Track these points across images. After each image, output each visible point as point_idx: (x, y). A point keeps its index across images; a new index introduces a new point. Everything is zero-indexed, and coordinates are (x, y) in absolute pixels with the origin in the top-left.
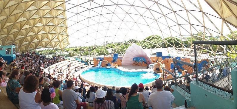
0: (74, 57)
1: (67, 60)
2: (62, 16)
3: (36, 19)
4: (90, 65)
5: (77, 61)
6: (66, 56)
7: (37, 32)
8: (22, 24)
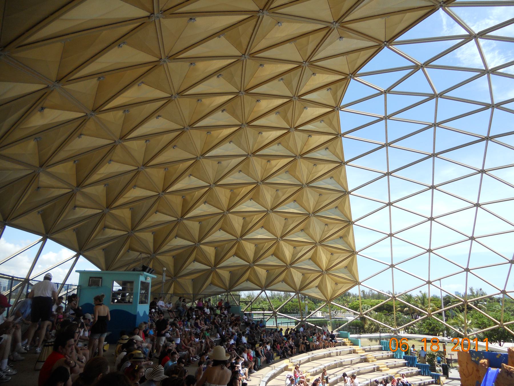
0: (377, 335)
1: (344, 344)
2: (329, 180)
3: (250, 216)
4: (443, 379)
5: (385, 354)
6: (343, 329)
7: (239, 232)
8: (188, 198)
